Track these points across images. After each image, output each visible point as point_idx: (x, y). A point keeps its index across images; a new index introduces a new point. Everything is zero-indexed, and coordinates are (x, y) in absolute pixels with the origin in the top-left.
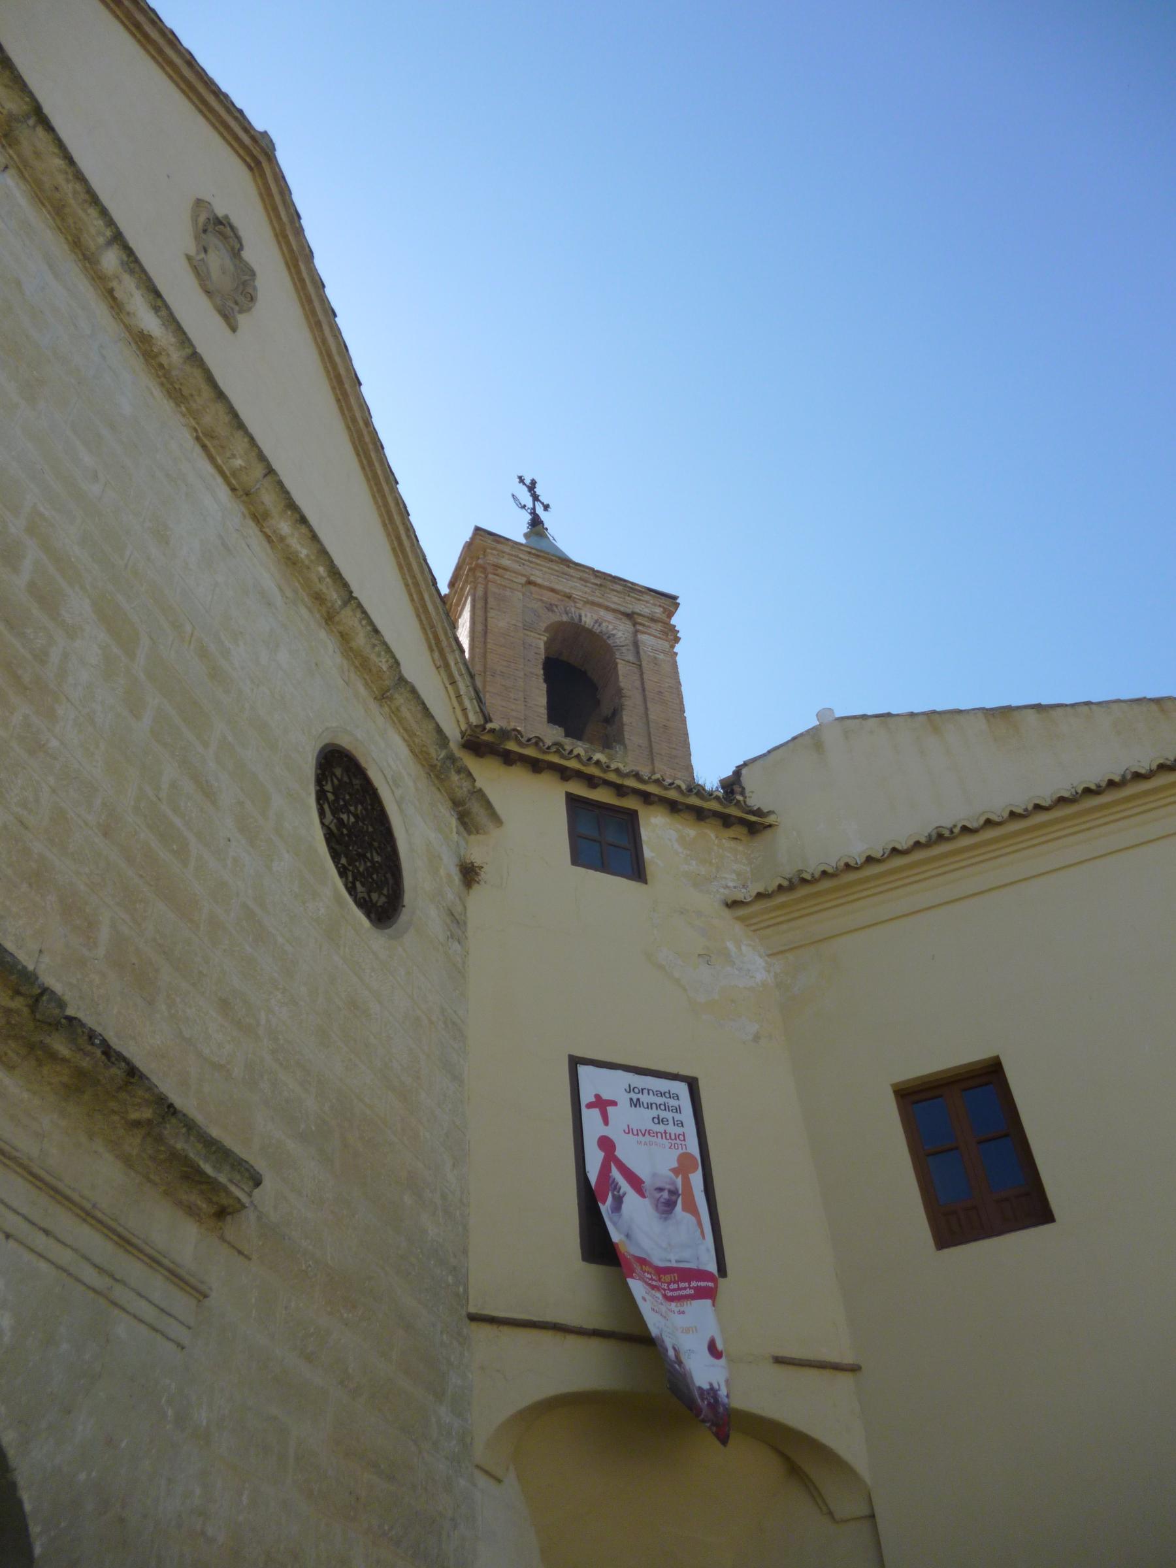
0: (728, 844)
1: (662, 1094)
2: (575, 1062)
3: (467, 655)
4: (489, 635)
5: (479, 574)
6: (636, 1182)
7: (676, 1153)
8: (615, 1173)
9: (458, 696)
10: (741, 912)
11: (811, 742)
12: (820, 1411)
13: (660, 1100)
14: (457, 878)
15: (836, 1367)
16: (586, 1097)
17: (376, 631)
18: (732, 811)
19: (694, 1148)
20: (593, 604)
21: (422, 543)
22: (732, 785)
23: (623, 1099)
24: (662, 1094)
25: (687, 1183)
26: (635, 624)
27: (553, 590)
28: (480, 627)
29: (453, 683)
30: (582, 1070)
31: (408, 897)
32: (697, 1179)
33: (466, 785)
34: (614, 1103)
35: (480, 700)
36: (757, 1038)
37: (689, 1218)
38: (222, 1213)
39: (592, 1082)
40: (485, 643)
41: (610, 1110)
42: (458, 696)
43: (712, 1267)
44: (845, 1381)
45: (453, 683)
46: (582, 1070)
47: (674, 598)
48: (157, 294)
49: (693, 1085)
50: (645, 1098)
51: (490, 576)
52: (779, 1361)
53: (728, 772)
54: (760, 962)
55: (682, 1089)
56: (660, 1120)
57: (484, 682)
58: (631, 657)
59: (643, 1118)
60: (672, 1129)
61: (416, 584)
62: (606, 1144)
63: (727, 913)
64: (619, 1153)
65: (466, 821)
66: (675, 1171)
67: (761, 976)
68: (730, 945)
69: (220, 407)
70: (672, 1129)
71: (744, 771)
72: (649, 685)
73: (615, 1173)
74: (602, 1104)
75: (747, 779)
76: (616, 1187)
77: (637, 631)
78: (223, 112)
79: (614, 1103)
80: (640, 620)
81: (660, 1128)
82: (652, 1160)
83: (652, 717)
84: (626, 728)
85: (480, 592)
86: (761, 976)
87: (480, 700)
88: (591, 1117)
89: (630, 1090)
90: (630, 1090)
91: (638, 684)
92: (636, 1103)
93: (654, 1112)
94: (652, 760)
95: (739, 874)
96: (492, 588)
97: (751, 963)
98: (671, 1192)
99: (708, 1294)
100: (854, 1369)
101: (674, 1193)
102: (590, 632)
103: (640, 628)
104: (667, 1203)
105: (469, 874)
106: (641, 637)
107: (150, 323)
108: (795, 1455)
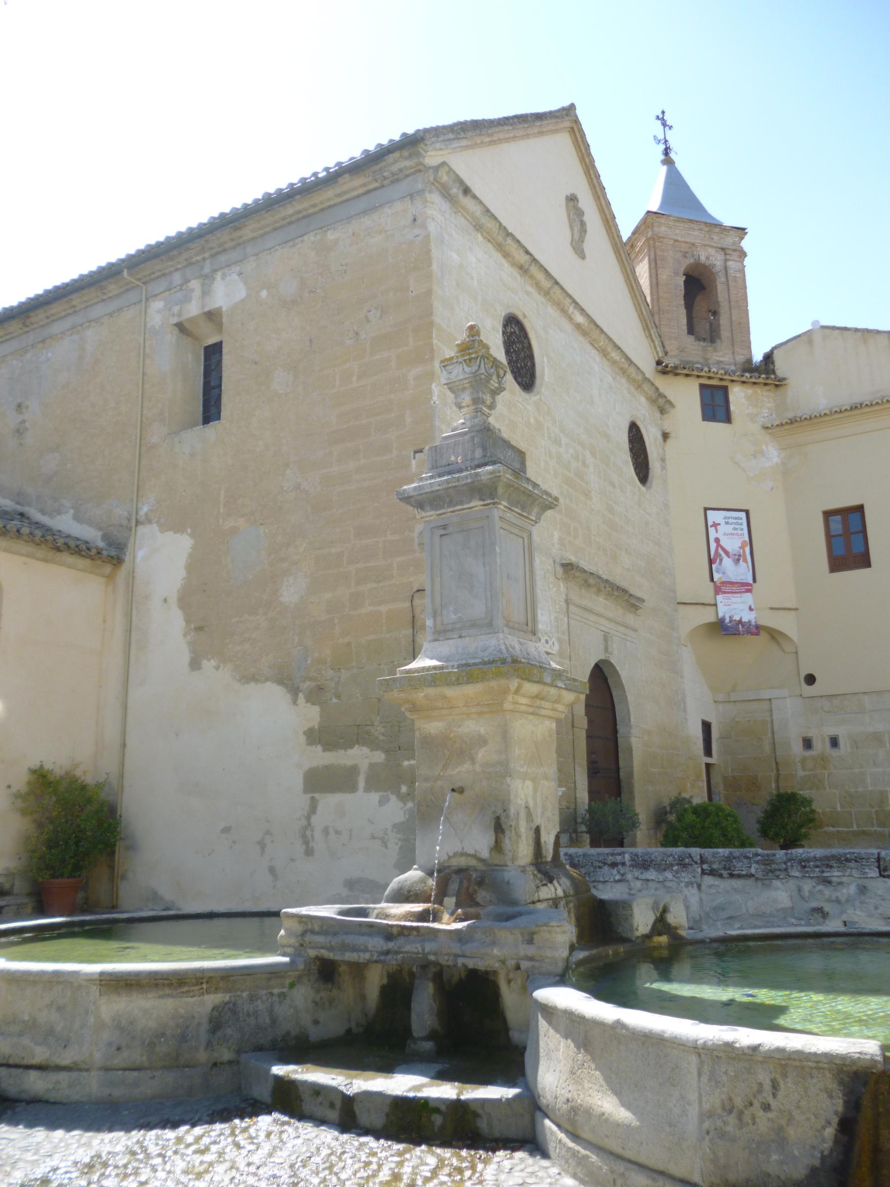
0: (765, 393)
1: (736, 518)
2: (706, 509)
3: (649, 299)
4: (660, 287)
5: (651, 242)
6: (727, 553)
7: (740, 541)
8: (720, 551)
9: (655, 347)
10: (770, 431)
11: (805, 339)
12: (784, 623)
13: (735, 521)
14: (660, 438)
15: (790, 609)
16: (710, 523)
17: (638, 368)
18: (765, 372)
19: (747, 539)
20: (705, 245)
21: (598, 164)
22: (768, 358)
23: (722, 522)
24: (736, 518)
25: (744, 552)
26: (726, 254)
27: (686, 242)
28: (654, 281)
29: (653, 341)
30: (709, 512)
31: (651, 474)
32: (748, 549)
33: (664, 400)
34: (719, 524)
35: (664, 346)
36: (772, 489)
37: (745, 564)
38: (292, 270)
39: (713, 516)
40: (658, 292)
41: (718, 527)
42: (655, 347)
43: (751, 581)
44: (793, 613)
45: (653, 341)
46: (709, 512)
47: (744, 229)
48: (583, 310)
49: (747, 512)
50: (730, 521)
51: (657, 244)
52: (772, 609)
53: (767, 349)
54: (776, 453)
55: (743, 515)
56: (735, 529)
57: (660, 321)
58: (723, 279)
59: (729, 529)
60: (740, 532)
61: (639, 304)
62: (717, 540)
63: (763, 431)
64: (722, 543)
65: (662, 411)
66: (740, 548)
67: (776, 460)
68: (764, 447)
69: (603, 336)
70: (740, 532)
71: (775, 352)
72: (733, 298)
73: (720, 551)
74: (715, 525)
75: (777, 356)
76: (720, 555)
77: (726, 260)
78: (580, 142)
79: (719, 524)
80: (728, 252)
81: (735, 532)
82: (732, 544)
83: (734, 318)
84: (722, 328)
85: (652, 256)
86: (776, 460)
87: (664, 346)
88: (712, 531)
89: (725, 518)
90: (725, 518)
91: (727, 297)
92: (727, 523)
93: (733, 526)
94: (733, 345)
95: (769, 409)
96: (659, 253)
97: (773, 454)
98: (740, 556)
99: (749, 591)
100: (796, 609)
101: (740, 556)
102: (704, 266)
103: (728, 257)
104: (737, 559)
105: (665, 436)
106: (730, 264)
107: (580, 319)
108: (774, 635)
